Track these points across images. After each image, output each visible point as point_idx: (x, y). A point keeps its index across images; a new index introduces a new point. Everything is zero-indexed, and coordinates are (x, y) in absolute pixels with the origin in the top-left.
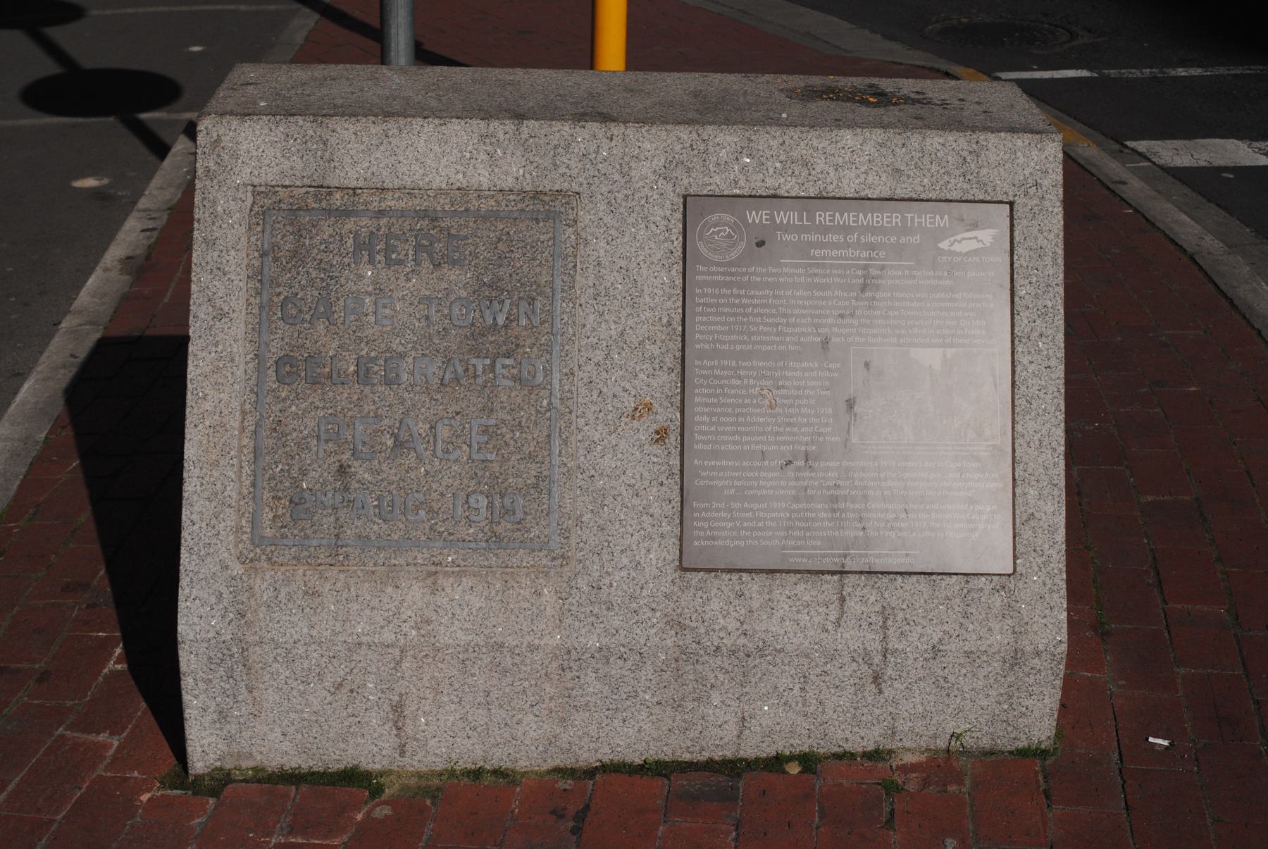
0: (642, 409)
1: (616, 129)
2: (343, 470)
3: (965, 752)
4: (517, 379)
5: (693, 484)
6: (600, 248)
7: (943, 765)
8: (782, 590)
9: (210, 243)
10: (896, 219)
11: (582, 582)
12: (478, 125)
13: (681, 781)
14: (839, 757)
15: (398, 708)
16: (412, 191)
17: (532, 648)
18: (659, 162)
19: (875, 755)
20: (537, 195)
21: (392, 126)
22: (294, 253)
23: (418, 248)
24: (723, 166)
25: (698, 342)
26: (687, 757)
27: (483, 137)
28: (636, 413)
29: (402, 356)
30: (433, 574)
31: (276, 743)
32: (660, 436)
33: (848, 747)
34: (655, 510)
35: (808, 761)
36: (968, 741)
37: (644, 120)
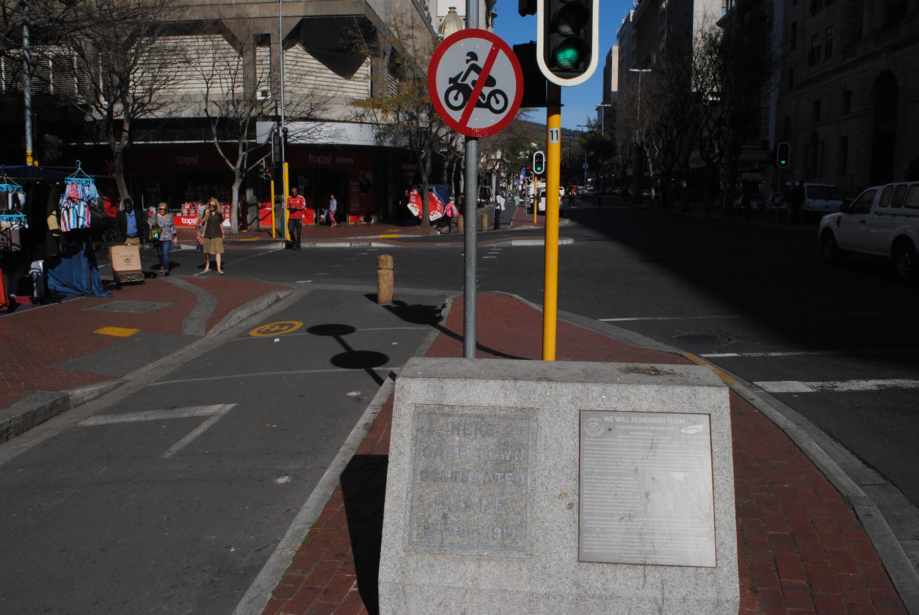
0: (563, 495)
1: (553, 384)
2: (445, 516)
4: (514, 482)
5: (584, 526)
6: (546, 430)
8: (621, 572)
9: (398, 425)
10: (664, 420)
12: (500, 382)
16: (474, 407)
20: (522, 409)
21: (467, 382)
22: (429, 430)
25: (586, 469)
30: (479, 560)
32: (570, 506)
34: (568, 536)
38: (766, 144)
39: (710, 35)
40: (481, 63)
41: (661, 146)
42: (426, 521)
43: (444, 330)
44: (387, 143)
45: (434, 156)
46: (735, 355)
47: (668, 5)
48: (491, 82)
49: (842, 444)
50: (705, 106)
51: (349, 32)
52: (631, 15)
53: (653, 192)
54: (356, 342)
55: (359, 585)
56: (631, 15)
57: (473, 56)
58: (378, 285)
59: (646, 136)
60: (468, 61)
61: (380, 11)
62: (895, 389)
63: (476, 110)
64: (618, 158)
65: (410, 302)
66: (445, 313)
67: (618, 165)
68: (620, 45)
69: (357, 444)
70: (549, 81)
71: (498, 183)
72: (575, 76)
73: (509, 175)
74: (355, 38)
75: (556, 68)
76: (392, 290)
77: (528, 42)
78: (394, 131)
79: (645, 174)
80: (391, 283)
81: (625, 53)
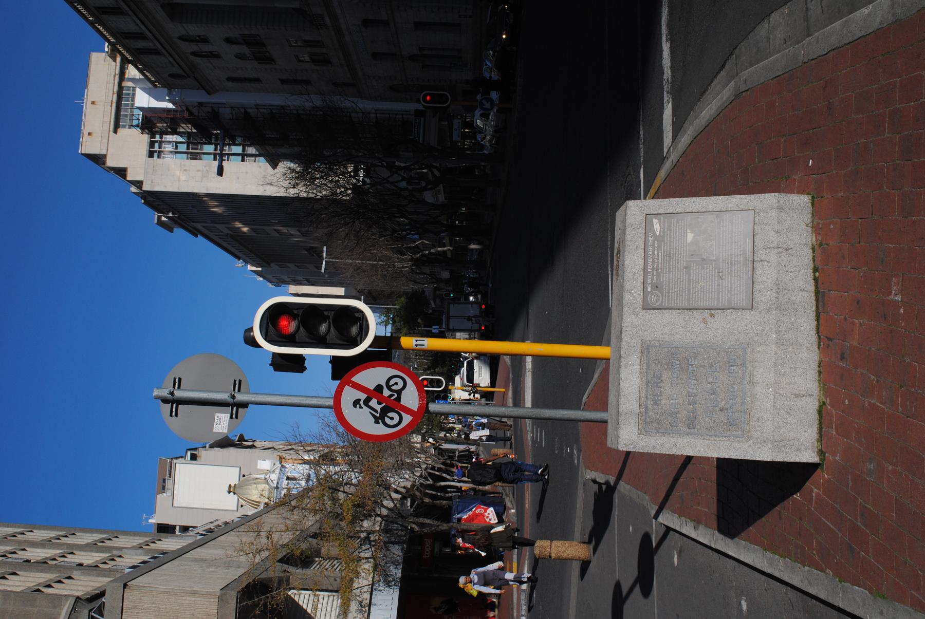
0: (704, 321)
1: (624, 329)
2: (721, 410)
3: (812, 222)
4: (695, 358)
5: (727, 305)
6: (657, 334)
7: (816, 229)
8: (759, 277)
9: (654, 448)
10: (650, 248)
11: (756, 339)
12: (622, 369)
13: (820, 308)
14: (814, 261)
15: (796, 396)
16: (640, 389)
17: (776, 353)
18: (633, 317)
19: (813, 249)
20: (642, 352)
21: (622, 394)
22: (658, 423)
23: (656, 387)
24: (635, 298)
25: (686, 305)
26: (814, 308)
27: (626, 367)
28: (706, 323)
29: (688, 392)
30: (753, 383)
31: (810, 434)
32: (712, 316)
33: (811, 258)
34: (734, 317)
35: (815, 270)
36: (809, 221)
37: (622, 322)
38: (418, 113)
39: (292, 179)
40: (363, 396)
41: (417, 237)
42: (725, 424)
43: (619, 478)
44: (397, 572)
45: (416, 514)
46: (642, 170)
47: (246, 224)
48: (379, 388)
49: (710, 84)
50: (372, 185)
51: (258, 612)
52: (254, 268)
53: (473, 246)
54: (629, 573)
55: (795, 493)
56: (254, 268)
57: (356, 403)
58: (571, 559)
59: (403, 254)
60: (361, 407)
61: (234, 574)
62: (669, 26)
63: (402, 402)
64: (428, 288)
65: (590, 523)
66: (601, 478)
67: (436, 289)
68: (288, 283)
69: (709, 531)
70: (369, 347)
71: (452, 441)
72: (367, 321)
73: (442, 429)
74: (265, 605)
75: (359, 339)
76: (575, 543)
77: (330, 365)
78: (382, 563)
79: (449, 255)
80: (567, 543)
81: (300, 278)
